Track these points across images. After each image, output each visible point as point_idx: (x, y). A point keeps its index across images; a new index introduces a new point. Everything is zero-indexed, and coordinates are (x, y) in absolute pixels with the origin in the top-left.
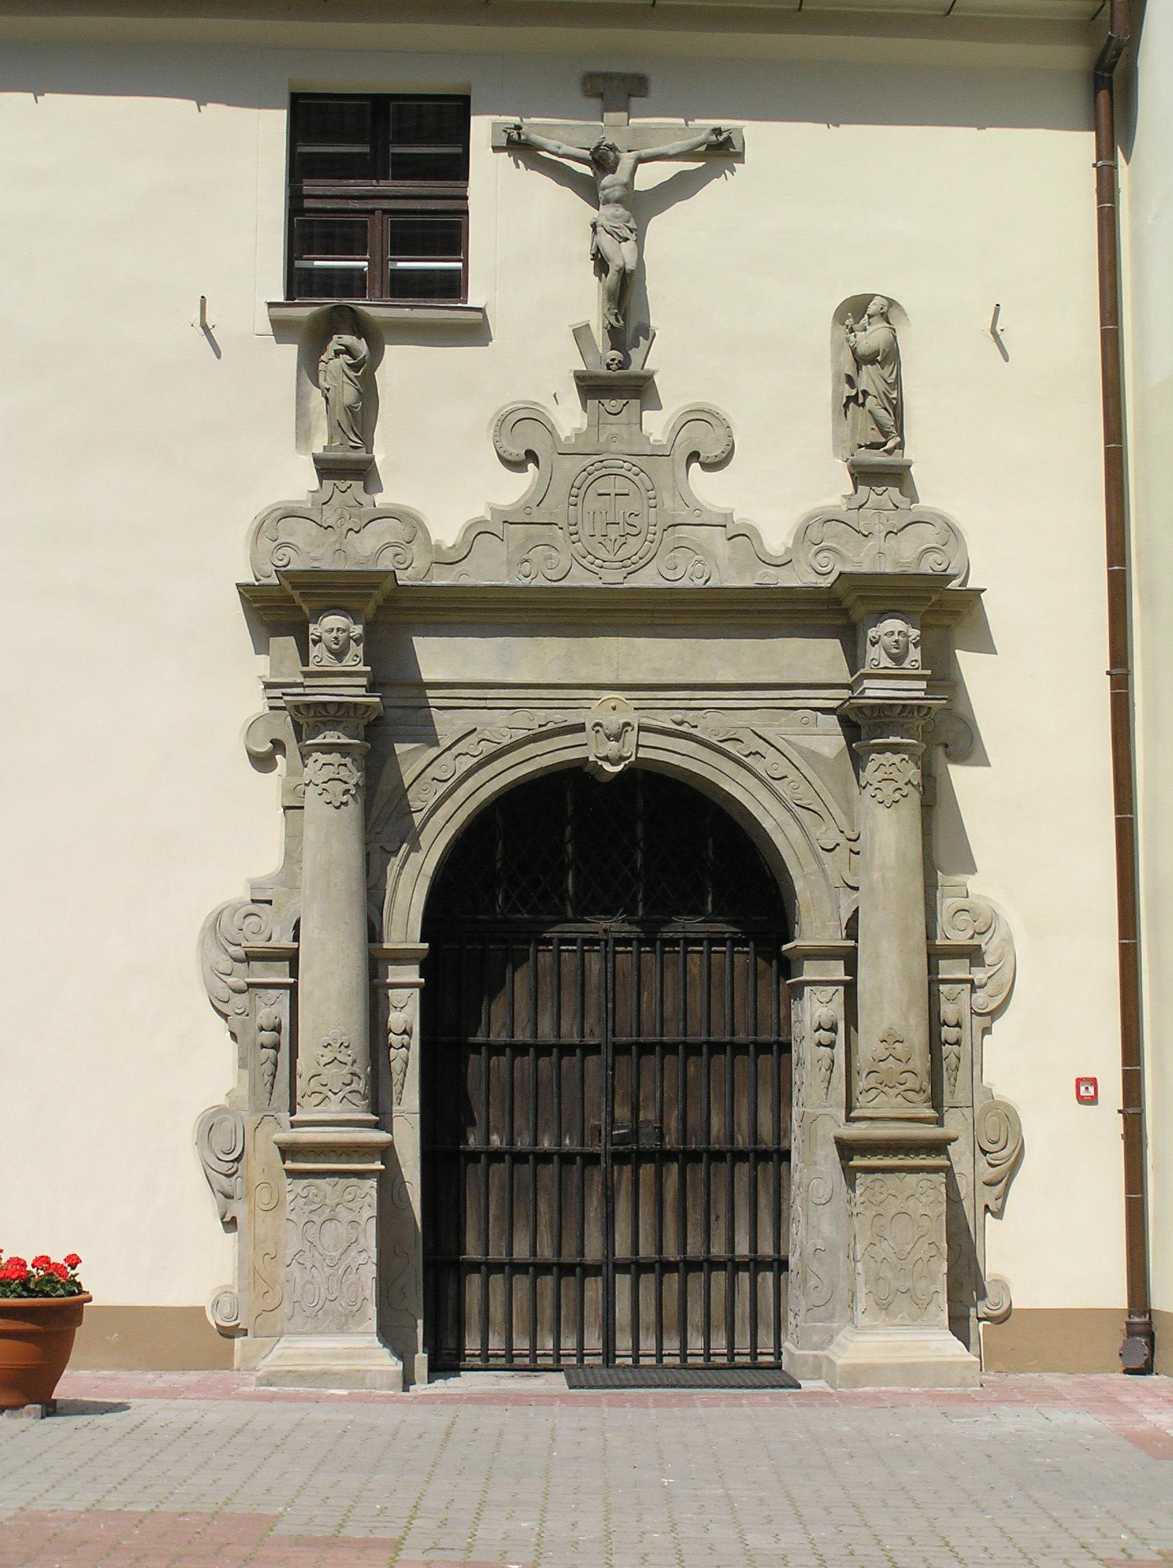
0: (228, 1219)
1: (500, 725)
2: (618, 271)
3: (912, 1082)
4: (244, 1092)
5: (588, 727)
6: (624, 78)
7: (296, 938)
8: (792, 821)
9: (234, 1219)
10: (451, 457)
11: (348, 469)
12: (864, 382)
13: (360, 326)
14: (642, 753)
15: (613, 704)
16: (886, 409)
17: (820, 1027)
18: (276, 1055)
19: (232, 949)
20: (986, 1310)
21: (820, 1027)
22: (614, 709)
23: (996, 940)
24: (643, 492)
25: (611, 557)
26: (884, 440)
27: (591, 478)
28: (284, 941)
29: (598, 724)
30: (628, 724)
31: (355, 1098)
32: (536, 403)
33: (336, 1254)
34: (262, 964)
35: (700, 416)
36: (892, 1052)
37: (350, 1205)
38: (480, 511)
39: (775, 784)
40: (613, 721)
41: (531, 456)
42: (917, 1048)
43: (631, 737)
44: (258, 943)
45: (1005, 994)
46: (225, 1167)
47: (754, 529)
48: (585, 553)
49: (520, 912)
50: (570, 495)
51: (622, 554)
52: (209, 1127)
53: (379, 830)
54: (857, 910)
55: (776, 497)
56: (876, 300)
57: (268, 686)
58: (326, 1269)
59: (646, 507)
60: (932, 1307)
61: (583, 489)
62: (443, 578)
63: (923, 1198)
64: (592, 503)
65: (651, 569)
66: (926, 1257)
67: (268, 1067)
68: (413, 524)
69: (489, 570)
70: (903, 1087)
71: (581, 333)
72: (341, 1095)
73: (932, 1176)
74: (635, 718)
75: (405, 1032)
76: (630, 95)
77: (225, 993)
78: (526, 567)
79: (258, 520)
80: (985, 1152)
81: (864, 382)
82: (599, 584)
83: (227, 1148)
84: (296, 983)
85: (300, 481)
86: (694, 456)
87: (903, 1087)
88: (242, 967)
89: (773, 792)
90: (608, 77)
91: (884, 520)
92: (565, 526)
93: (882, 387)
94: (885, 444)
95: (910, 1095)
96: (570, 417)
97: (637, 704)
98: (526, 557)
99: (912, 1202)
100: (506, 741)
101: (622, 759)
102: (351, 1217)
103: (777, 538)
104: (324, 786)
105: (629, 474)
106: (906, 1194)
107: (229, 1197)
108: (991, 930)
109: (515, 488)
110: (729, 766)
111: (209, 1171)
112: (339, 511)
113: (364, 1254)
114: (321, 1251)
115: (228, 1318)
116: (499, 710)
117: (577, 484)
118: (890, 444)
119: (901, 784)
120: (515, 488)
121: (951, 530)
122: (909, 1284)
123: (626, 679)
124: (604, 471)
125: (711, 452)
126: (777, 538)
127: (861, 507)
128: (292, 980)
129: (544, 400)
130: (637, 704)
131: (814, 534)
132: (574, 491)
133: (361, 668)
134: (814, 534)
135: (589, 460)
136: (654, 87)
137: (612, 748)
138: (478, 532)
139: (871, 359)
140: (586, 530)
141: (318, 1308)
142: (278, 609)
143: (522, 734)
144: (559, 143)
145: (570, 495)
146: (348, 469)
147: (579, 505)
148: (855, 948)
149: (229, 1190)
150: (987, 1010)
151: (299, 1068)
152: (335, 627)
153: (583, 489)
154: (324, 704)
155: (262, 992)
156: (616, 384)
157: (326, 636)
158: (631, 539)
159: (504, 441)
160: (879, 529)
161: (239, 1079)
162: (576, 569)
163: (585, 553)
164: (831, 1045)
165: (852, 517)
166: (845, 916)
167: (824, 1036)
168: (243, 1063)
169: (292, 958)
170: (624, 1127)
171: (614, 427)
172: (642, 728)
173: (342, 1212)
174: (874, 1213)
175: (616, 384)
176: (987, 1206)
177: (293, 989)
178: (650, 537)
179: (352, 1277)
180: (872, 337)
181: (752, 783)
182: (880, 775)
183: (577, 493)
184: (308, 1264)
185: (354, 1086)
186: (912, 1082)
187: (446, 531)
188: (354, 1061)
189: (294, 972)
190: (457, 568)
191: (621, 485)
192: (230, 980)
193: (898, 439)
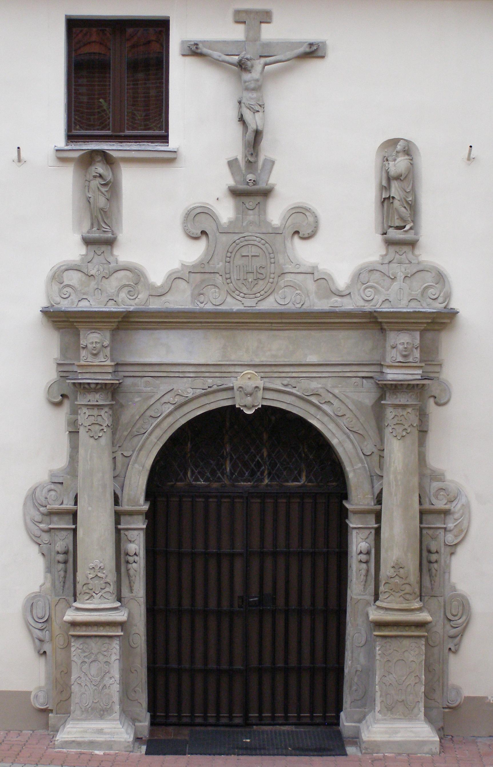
0: (42, 652)
1: (187, 388)
2: (254, 131)
3: (408, 589)
4: (48, 585)
5: (235, 388)
6: (257, 12)
7: (76, 503)
8: (347, 440)
9: (45, 652)
10: (164, 217)
11: (101, 240)
12: (394, 192)
13: (106, 158)
14: (265, 404)
15: (249, 376)
16: (405, 207)
17: (361, 553)
18: (65, 564)
19: (42, 509)
20: (448, 704)
21: (361, 553)
22: (249, 378)
23: (459, 506)
24: (267, 254)
25: (250, 292)
26: (402, 224)
27: (238, 247)
28: (68, 505)
29: (240, 387)
30: (257, 387)
31: (107, 596)
32: (208, 204)
33: (98, 679)
34: (56, 521)
35: (300, 211)
36: (398, 574)
37: (105, 653)
38: (176, 266)
39: (338, 420)
40: (250, 385)
41: (203, 233)
42: (412, 570)
43: (260, 394)
44: (56, 506)
45: (463, 535)
46: (40, 626)
47: (329, 275)
48: (234, 289)
49: (200, 481)
50: (227, 257)
51: (255, 290)
52: (31, 605)
53: (121, 444)
54: (382, 489)
55: (342, 254)
56: (401, 143)
57: (59, 364)
58: (92, 686)
59: (269, 263)
60: (416, 710)
61: (234, 253)
62: (155, 305)
63: (412, 652)
64: (239, 261)
65: (271, 299)
66: (413, 684)
67: (62, 573)
68: (137, 275)
69: (181, 300)
70: (403, 592)
71: (232, 164)
72: (100, 594)
73: (418, 640)
74: (261, 384)
75: (135, 554)
76: (261, 22)
77: (38, 533)
78: (202, 298)
79: (52, 271)
80: (450, 620)
81: (394, 192)
82: (241, 307)
83: (40, 616)
84: (76, 527)
85: (74, 251)
86: (297, 232)
87: (403, 592)
88: (47, 519)
89: (337, 425)
90: (247, 12)
91: (403, 270)
92: (223, 274)
93: (403, 195)
94: (404, 227)
95: (408, 596)
96: (226, 211)
97: (262, 375)
98: (202, 292)
99: (406, 654)
100: (190, 396)
101: (253, 406)
102: (105, 660)
103: (342, 280)
104: (89, 427)
105: (260, 245)
106: (403, 650)
107: (41, 641)
108: (457, 500)
109: (194, 252)
110: (313, 410)
111: (31, 627)
112: (97, 266)
113: (113, 679)
114: (90, 677)
115: (42, 705)
116: (187, 374)
117: (230, 250)
118: (407, 227)
119: (406, 426)
120: (194, 252)
121: (440, 277)
122: (403, 697)
123: (257, 361)
124: (246, 243)
125: (305, 232)
126: (342, 280)
127: (390, 262)
128: (74, 527)
129: (211, 202)
130: (262, 375)
131: (364, 277)
132: (229, 254)
133: (108, 363)
134: (364, 277)
135: (236, 237)
136: (276, 18)
137: (249, 400)
138: (175, 278)
139: (398, 178)
140: (234, 277)
141: (88, 706)
142: (63, 321)
143: (199, 392)
144: (220, 54)
145: (227, 257)
146: (101, 240)
147: (231, 262)
148: (381, 510)
149: (42, 637)
150: (454, 543)
151: (78, 579)
152: (94, 341)
153: (234, 253)
154: (89, 384)
155: (57, 533)
156: (251, 193)
157: (90, 346)
158: (261, 282)
159: (189, 226)
160: (400, 276)
161: (46, 578)
162: (229, 299)
163: (234, 289)
164: (367, 562)
165: (384, 268)
166: (377, 492)
167: (363, 557)
168: (49, 569)
169: (74, 515)
170: (256, 597)
171: (251, 216)
172: (265, 389)
173: (101, 658)
174: (385, 660)
175: (251, 193)
176: (450, 649)
177: (75, 531)
178: (271, 280)
179: (106, 691)
180: (399, 165)
181: (326, 419)
182: (395, 421)
183: (229, 255)
184: (83, 684)
185: (107, 589)
186: (408, 589)
187: (157, 277)
188: (107, 576)
189: (75, 522)
190: (163, 298)
191: (254, 251)
192: (41, 526)
193: (412, 224)
